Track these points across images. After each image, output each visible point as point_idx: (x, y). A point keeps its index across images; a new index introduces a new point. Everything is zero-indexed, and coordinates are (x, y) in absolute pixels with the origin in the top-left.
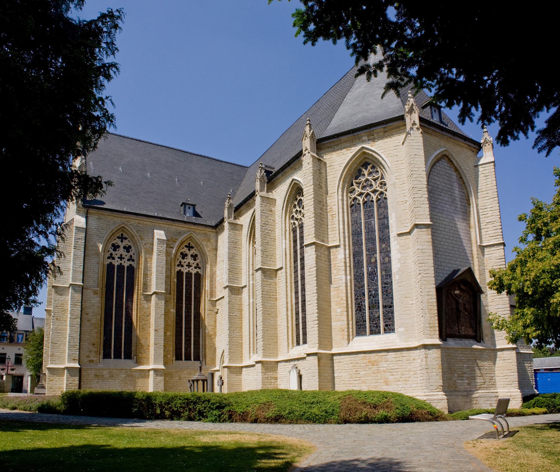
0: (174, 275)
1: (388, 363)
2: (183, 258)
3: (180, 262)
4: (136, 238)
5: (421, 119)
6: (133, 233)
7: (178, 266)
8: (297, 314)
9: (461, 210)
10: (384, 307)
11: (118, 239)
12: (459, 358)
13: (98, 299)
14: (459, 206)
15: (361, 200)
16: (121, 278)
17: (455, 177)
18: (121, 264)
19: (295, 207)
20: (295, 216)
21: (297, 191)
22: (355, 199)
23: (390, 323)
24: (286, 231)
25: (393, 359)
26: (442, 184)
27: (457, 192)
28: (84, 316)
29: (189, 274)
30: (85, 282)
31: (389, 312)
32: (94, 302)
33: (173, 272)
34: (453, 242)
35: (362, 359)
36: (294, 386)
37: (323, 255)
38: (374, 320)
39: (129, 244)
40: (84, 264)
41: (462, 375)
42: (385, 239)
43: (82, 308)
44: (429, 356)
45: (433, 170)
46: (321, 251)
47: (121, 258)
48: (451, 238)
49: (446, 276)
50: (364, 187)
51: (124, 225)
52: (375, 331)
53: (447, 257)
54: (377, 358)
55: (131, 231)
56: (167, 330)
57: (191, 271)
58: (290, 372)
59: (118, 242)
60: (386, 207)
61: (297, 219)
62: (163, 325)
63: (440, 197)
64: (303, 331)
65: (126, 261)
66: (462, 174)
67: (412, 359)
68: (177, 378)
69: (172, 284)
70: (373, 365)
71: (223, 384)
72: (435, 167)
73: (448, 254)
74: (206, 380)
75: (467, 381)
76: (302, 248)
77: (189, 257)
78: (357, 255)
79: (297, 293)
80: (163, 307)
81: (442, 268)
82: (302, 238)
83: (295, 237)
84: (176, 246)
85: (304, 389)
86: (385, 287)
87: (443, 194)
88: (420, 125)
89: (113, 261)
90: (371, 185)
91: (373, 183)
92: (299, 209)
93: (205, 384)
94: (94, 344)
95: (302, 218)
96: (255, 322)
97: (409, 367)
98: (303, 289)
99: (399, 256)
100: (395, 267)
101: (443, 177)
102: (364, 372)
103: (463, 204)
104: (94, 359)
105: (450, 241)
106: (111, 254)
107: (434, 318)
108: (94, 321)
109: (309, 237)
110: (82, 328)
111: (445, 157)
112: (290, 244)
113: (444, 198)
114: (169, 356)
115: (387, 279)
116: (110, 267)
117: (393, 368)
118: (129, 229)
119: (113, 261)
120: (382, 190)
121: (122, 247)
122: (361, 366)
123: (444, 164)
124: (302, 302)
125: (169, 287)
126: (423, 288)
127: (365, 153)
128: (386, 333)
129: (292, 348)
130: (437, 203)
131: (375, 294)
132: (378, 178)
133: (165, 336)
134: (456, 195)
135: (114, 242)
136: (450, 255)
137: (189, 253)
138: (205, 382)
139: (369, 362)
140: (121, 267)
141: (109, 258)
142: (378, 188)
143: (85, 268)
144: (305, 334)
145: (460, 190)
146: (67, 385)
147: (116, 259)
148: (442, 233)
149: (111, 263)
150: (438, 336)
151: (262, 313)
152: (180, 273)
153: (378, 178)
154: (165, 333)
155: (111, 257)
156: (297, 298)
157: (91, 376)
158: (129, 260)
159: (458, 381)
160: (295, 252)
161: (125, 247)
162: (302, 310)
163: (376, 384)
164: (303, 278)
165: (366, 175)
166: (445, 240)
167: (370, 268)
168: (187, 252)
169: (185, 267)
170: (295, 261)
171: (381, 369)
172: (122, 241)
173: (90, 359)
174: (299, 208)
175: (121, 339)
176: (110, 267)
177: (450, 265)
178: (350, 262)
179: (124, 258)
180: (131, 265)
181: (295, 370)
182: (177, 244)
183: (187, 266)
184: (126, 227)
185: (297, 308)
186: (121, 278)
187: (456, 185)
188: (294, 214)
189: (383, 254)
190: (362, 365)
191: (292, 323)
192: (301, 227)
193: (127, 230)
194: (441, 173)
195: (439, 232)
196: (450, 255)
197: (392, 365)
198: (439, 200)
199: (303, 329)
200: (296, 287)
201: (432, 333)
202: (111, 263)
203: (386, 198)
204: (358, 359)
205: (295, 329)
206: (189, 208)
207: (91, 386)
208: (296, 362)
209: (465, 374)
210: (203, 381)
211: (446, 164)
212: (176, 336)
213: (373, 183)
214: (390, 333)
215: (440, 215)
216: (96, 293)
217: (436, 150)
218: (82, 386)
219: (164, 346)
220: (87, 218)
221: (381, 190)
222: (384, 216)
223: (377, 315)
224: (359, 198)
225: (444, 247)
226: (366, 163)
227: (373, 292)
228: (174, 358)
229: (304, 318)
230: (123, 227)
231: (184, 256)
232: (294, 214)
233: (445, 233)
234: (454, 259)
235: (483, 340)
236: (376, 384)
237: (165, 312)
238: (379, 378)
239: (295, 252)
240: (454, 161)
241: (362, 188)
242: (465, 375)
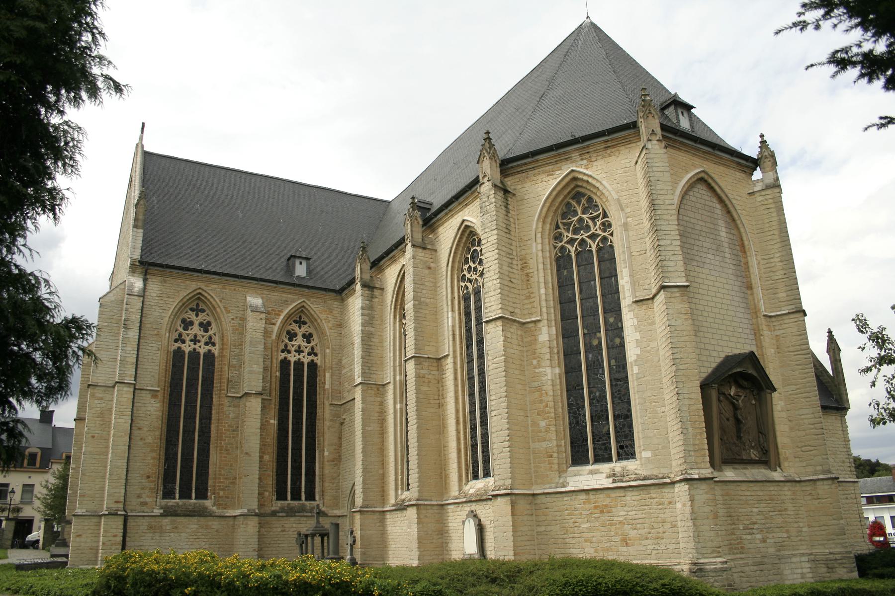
0: (276, 365)
1: (626, 508)
2: (290, 340)
3: (286, 346)
4: (218, 309)
5: (664, 128)
6: (214, 303)
7: (283, 351)
8: (473, 428)
9: (732, 262)
10: (616, 417)
11: (190, 312)
12: (744, 498)
13: (158, 405)
14: (727, 255)
15: (573, 250)
16: (193, 369)
17: (718, 212)
18: (195, 349)
19: (466, 262)
20: (468, 276)
21: (469, 238)
22: (562, 247)
23: (628, 443)
24: (453, 299)
25: (636, 503)
26: (700, 223)
27: (723, 234)
28: (136, 432)
29: (299, 364)
30: (138, 379)
31: (624, 426)
32: (152, 409)
33: (275, 361)
34: (722, 312)
35: (584, 503)
36: (471, 548)
37: (515, 337)
38: (601, 438)
39: (208, 319)
40: (138, 351)
41: (750, 526)
42: (614, 308)
43: (132, 420)
44: (696, 498)
45: (684, 202)
46: (511, 330)
47: (195, 340)
48: (719, 306)
49: (714, 365)
50: (576, 231)
51: (200, 291)
52: (603, 457)
53: (715, 336)
54: (608, 501)
55: (211, 300)
56: (264, 453)
57: (303, 360)
58: (464, 522)
59: (192, 316)
60: (613, 260)
61: (470, 281)
62: (258, 446)
63: (697, 243)
64: (483, 456)
65: (203, 346)
66: (730, 206)
67: (666, 503)
68: (279, 529)
69: (274, 379)
70: (602, 512)
71: (354, 542)
72: (687, 197)
73: (714, 331)
74: (327, 535)
75: (759, 536)
76: (479, 323)
77: (299, 337)
78: (568, 334)
79: (472, 395)
80: (259, 417)
81: (707, 353)
82: (479, 309)
83: (467, 307)
84: (280, 321)
85: (491, 554)
86: (616, 385)
87: (701, 238)
88: (663, 136)
89: (182, 346)
90: (588, 228)
91: (591, 223)
92: (473, 266)
93: (326, 541)
94: (148, 477)
95: (479, 279)
96: (404, 440)
97: (662, 515)
98: (483, 390)
99: (637, 336)
100: (632, 352)
101: (700, 211)
102: (588, 525)
103: (735, 252)
104: (148, 500)
105: (717, 311)
106: (180, 335)
107: (701, 434)
108: (150, 439)
109: (492, 306)
110: (131, 451)
111: (703, 180)
112: (460, 318)
113: (705, 244)
114: (267, 494)
115: (619, 372)
116: (178, 354)
117: (637, 517)
118: (209, 297)
119: (182, 346)
120: (606, 234)
121: (197, 323)
122: (581, 514)
123: (702, 192)
124: (481, 409)
125: (268, 385)
126: (680, 385)
127: (575, 179)
128: (622, 459)
129: (466, 484)
130: (694, 252)
131: (600, 396)
132: (598, 216)
133: (261, 461)
134: (723, 239)
135: (186, 316)
136: (719, 332)
137: (300, 332)
138: (326, 538)
139: (596, 507)
140: (194, 354)
141: (176, 341)
142: (599, 232)
143: (140, 356)
144: (486, 461)
145: (728, 231)
146: (103, 543)
147: (188, 342)
148: (705, 297)
149: (179, 348)
150: (708, 465)
151: (418, 428)
152: (285, 363)
153: (598, 216)
154: (261, 457)
155: (180, 339)
156: (472, 404)
157: (142, 527)
158: (206, 344)
159: (744, 537)
160: (469, 330)
161: (201, 324)
162: (482, 422)
163: (608, 544)
164: (482, 372)
165: (579, 212)
166: (709, 309)
167: (590, 356)
168: (297, 329)
169: (293, 353)
170: (469, 346)
171: (615, 519)
172: (197, 315)
173: (142, 500)
174: (474, 263)
175: (192, 467)
176: (178, 354)
177: (720, 349)
178: (558, 346)
179: (199, 341)
180: (210, 351)
181: (471, 520)
182: (281, 317)
183: (296, 351)
184: (204, 293)
185: (473, 419)
186: (193, 369)
187: (721, 223)
188: (465, 272)
189: (610, 333)
190: (584, 512)
191: (466, 443)
192: (477, 292)
193: (206, 297)
194: (698, 205)
195: (699, 296)
196: (719, 332)
197: (634, 513)
198: (696, 248)
199: (483, 452)
200: (471, 386)
201: (699, 460)
202: (179, 348)
203: (612, 247)
204: (576, 502)
205: (470, 453)
206: (301, 263)
207: (141, 544)
208: (474, 507)
209: (755, 523)
210: (322, 536)
211: (704, 192)
212: (277, 462)
213: (591, 223)
214: (628, 459)
215: (700, 270)
216: (154, 394)
217: (687, 172)
218: (128, 544)
219: (260, 479)
220: (145, 280)
221: (603, 234)
222: (610, 273)
223: (605, 430)
224: (569, 246)
225: (708, 319)
226: (576, 198)
227: (597, 394)
228: (274, 498)
229: (485, 435)
230: (200, 293)
231: (292, 336)
232: (465, 272)
233: (710, 298)
234: (725, 338)
235: (780, 466)
236: (608, 544)
237: (262, 425)
238: (613, 533)
239: (469, 330)
240: (716, 188)
241: (574, 233)
242: (756, 526)
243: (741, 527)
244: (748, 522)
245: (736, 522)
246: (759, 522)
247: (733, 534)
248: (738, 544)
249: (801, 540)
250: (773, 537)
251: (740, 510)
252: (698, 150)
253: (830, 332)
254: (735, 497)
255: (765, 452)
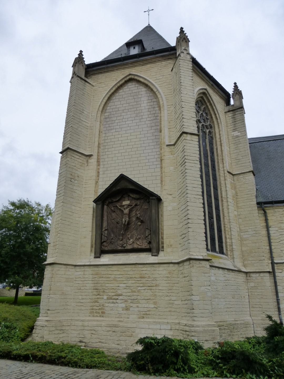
12: (113, 276)
159: (107, 305)
219: (117, 370)
243: (105, 297)
244: (113, 294)
245: (102, 293)
246: (124, 294)
247: (96, 302)
248: (99, 309)
249: (170, 311)
250: (138, 307)
251: (107, 285)
252: (127, 64)
253: (235, 83)
254: (104, 276)
255: (154, 245)
